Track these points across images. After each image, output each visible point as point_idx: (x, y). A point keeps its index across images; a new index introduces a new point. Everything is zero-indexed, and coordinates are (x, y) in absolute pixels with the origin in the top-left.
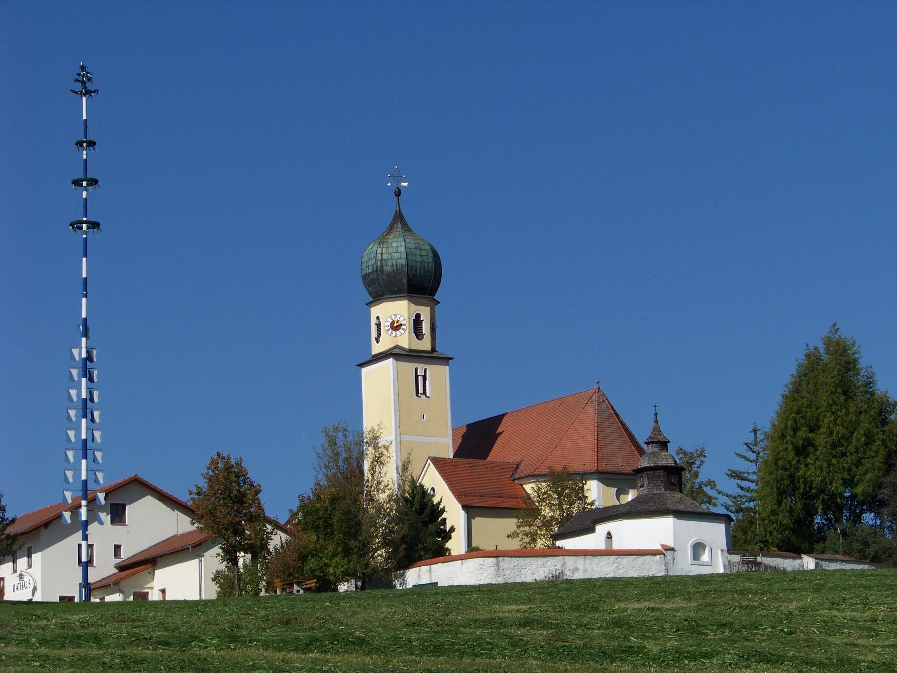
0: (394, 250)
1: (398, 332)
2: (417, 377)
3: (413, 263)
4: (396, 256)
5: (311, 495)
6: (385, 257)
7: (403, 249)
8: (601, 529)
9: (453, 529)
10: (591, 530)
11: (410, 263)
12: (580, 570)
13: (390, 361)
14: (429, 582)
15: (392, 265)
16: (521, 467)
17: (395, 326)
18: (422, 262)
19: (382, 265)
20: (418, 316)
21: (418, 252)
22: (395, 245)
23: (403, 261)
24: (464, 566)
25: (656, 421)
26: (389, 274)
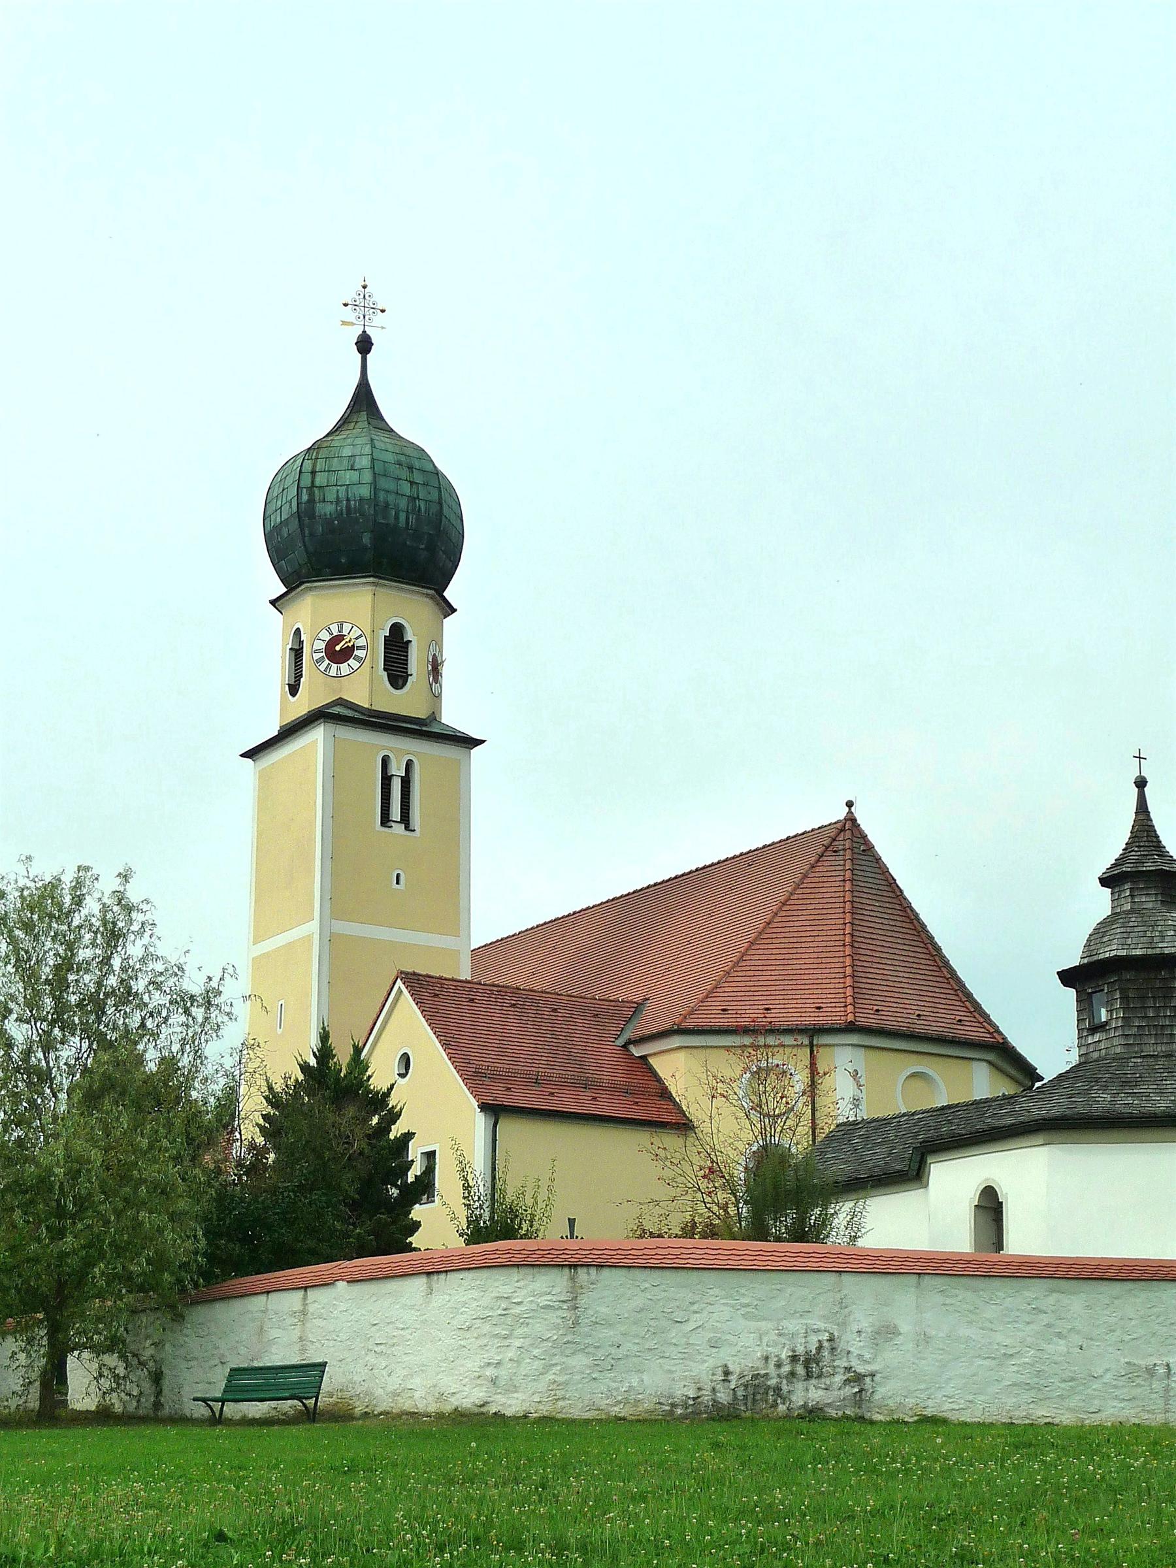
0: (345, 464)
1: (344, 667)
2: (386, 780)
3: (391, 499)
4: (349, 477)
5: (269, 1109)
6: (320, 480)
7: (365, 462)
8: (955, 1181)
9: (413, 1161)
10: (911, 1175)
11: (382, 496)
12: (946, 1364)
13: (318, 735)
14: (295, 1360)
15: (338, 501)
16: (648, 1010)
17: (338, 652)
18: (413, 499)
19: (311, 501)
20: (397, 631)
21: (404, 473)
22: (347, 452)
23: (365, 492)
24: (438, 1300)
25: (1142, 808)
26: (328, 522)
